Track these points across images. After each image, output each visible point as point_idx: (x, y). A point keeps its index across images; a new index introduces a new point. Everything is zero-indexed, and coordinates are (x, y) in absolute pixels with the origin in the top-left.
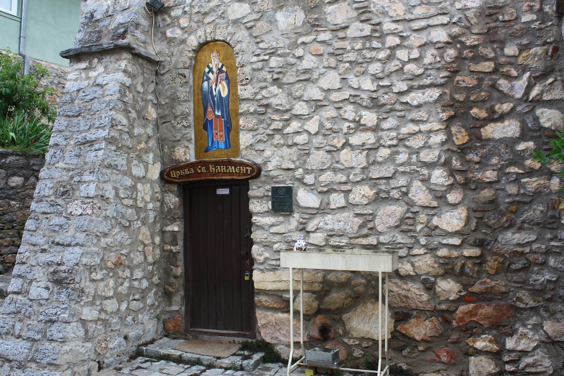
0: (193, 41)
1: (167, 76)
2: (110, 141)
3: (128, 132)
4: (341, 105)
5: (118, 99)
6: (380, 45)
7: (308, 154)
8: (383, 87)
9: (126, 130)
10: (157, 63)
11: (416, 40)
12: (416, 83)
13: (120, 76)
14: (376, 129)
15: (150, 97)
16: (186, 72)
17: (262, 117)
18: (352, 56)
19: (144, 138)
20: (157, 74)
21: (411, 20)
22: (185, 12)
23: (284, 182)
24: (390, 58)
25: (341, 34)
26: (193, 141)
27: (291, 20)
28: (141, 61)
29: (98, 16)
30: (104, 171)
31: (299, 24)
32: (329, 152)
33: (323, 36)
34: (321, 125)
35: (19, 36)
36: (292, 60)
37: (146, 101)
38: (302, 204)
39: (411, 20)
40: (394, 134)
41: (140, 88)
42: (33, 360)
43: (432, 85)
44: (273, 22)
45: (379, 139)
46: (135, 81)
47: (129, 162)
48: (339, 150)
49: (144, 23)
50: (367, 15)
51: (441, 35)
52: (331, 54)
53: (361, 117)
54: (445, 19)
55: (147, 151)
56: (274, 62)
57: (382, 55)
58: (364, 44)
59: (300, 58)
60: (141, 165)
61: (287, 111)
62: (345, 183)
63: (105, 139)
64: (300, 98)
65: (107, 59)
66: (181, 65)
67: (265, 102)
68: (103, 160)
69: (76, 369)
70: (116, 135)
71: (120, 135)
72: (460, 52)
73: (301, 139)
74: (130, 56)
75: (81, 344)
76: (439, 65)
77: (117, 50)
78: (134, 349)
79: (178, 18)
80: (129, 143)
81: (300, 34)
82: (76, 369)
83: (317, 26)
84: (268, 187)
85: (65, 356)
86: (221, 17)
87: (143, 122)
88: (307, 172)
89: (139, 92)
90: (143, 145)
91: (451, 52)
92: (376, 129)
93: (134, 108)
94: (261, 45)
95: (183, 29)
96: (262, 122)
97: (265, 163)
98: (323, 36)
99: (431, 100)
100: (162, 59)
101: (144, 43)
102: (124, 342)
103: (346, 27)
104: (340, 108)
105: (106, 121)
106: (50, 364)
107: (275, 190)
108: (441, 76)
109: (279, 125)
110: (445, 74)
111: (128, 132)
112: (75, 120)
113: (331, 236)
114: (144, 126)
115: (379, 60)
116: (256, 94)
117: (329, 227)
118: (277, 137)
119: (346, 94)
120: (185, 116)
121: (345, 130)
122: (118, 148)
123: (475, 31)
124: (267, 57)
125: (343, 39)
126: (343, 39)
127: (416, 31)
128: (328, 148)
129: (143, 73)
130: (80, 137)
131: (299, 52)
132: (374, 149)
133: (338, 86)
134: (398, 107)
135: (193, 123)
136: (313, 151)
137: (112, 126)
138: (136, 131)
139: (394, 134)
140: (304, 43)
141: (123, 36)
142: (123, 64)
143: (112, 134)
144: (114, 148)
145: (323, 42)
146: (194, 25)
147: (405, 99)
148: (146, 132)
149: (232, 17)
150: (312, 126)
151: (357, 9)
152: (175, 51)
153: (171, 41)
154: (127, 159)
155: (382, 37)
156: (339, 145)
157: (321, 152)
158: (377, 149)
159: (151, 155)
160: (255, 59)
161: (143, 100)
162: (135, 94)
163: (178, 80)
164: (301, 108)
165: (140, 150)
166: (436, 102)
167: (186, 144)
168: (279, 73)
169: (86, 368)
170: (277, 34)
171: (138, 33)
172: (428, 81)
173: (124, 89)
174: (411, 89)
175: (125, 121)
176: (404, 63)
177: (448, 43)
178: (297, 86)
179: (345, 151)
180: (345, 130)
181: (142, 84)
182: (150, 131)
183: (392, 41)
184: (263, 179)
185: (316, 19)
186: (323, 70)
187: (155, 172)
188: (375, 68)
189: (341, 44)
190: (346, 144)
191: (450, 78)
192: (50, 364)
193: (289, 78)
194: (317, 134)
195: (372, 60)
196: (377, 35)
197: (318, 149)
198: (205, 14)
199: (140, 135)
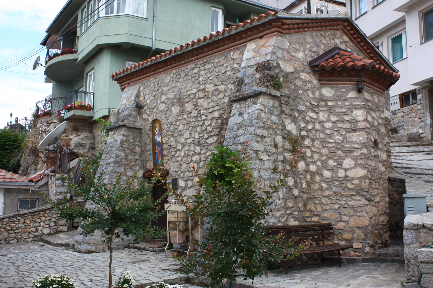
0: (151, 120)
1: (144, 134)
2: (116, 162)
3: (125, 159)
4: (190, 144)
5: (120, 146)
6: (200, 120)
7: (181, 165)
8: (201, 136)
9: (124, 158)
10: (141, 129)
11: (210, 117)
12: (210, 135)
13: (121, 137)
14: (200, 154)
15: (137, 143)
16: (149, 132)
17: (169, 150)
18: (192, 125)
19: (134, 160)
20: (141, 133)
21: (208, 109)
22: (148, 108)
23: (175, 176)
24: (203, 124)
25: (189, 115)
26: (152, 161)
27: (176, 110)
28: (132, 129)
29: (120, 112)
30: (112, 174)
31: (178, 112)
32: (187, 164)
33: (185, 117)
34: (185, 153)
35: (361, 17)
36: (176, 127)
37: (135, 145)
38: (180, 186)
39: (208, 109)
40: (204, 156)
41: (131, 140)
42: (83, 242)
43: (214, 135)
44: (171, 111)
45: (200, 158)
46: (129, 138)
47: (125, 170)
48: (190, 163)
49: (134, 113)
50: (197, 107)
51: (216, 114)
52: (187, 124)
53: (195, 149)
54: (218, 108)
55: (135, 165)
56: (172, 127)
57: (201, 124)
58: (196, 119)
59: (178, 126)
60: (132, 171)
61: (176, 147)
62: (191, 176)
63: (113, 162)
64: (179, 142)
65: (119, 130)
66: (147, 130)
67: (169, 144)
68: (112, 170)
69: (97, 246)
70: (119, 160)
71: (121, 160)
72: (222, 121)
73: (179, 159)
74: (126, 128)
75: (100, 238)
76: (216, 127)
77: (121, 127)
78: (127, 244)
79: (146, 110)
80: (125, 163)
81: (178, 116)
82: (97, 246)
83: (183, 112)
84: (171, 179)
85: (93, 241)
86: (157, 110)
87: (133, 154)
88: (181, 172)
89: (131, 142)
90: (133, 163)
91: (220, 121)
92: (200, 154)
93: (128, 149)
94: (169, 121)
95: (148, 114)
96: (169, 152)
97: (170, 169)
98: (185, 117)
99: (215, 141)
100: (141, 127)
101: (134, 121)
102: (121, 241)
103: (191, 113)
104: (189, 146)
105: (114, 155)
106: (87, 243)
107: (173, 180)
108: (216, 131)
109: (173, 153)
110: (218, 130)
111: (125, 159)
112: (107, 155)
113: (189, 198)
114: (134, 156)
115: (200, 126)
116: (167, 141)
117: (188, 195)
118: (173, 158)
119: (191, 140)
120: (149, 150)
121: (191, 155)
122: (120, 165)
123: (227, 112)
124: (170, 126)
125: (190, 117)
126: (190, 117)
127: (210, 113)
128: (187, 162)
129: (133, 134)
130: (107, 161)
131: (178, 123)
132: (199, 162)
133: (189, 137)
134: (206, 145)
135: (152, 153)
136: (183, 164)
137: (117, 157)
138: (129, 158)
139: (204, 156)
140: (179, 120)
141: (123, 121)
142: (122, 132)
143: (117, 160)
144: (117, 165)
145: (185, 119)
146: (150, 113)
147: (208, 141)
148: (135, 158)
149: (160, 109)
150: (182, 154)
151: (194, 105)
152: (146, 123)
153: (145, 119)
154: (124, 169)
155: (201, 116)
156: (190, 161)
157: (185, 164)
158: (200, 162)
159: (138, 167)
160: (167, 127)
161: (133, 145)
162: (129, 143)
163: (147, 136)
164: (179, 147)
165: (131, 165)
166: (216, 142)
167: (150, 162)
168: (173, 132)
169: (102, 247)
170: (172, 116)
171: (131, 119)
172: (213, 134)
173: (122, 142)
174: (209, 137)
175: (123, 154)
176: (207, 126)
177: (219, 117)
178: (178, 137)
179: (191, 163)
180: (191, 155)
181: (133, 139)
182: (137, 157)
183: (204, 117)
184: (170, 175)
185: (183, 110)
186: (185, 130)
187: (140, 174)
188: (199, 129)
189: (189, 119)
190: (192, 161)
191: (220, 131)
192: (87, 243)
193: (176, 134)
194: (184, 156)
195: (198, 126)
196: (199, 115)
197: (184, 162)
198: (153, 108)
199: (131, 159)
